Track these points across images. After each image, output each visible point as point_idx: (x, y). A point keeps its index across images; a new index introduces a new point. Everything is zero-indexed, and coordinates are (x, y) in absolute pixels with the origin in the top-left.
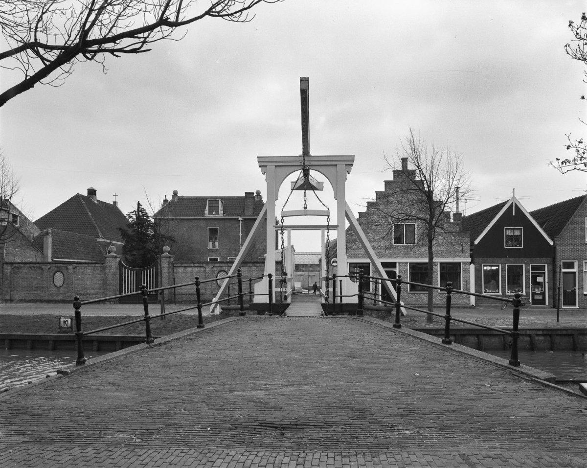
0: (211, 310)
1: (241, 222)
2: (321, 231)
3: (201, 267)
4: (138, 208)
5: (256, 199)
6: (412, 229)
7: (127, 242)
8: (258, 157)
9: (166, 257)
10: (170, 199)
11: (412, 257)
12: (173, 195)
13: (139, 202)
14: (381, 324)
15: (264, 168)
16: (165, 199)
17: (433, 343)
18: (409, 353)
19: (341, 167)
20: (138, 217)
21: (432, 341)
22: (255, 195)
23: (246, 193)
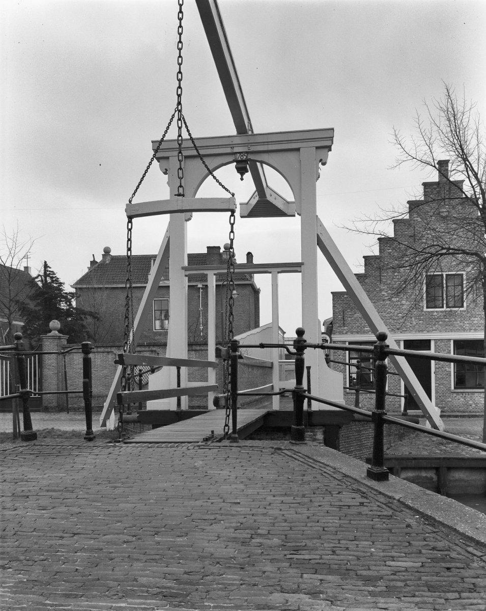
0: (101, 422)
1: (201, 291)
2: (269, 275)
3: (108, 352)
4: (45, 271)
5: (224, 256)
6: (457, 281)
7: (29, 323)
8: (152, 142)
9: (54, 337)
10: (99, 259)
11: (458, 330)
12: (104, 253)
13: (45, 262)
14: (337, 465)
15: (164, 162)
16: (92, 260)
17: (471, 539)
18: (381, 586)
19: (308, 151)
20: (45, 283)
21: (470, 533)
22: (222, 250)
23: (208, 247)
